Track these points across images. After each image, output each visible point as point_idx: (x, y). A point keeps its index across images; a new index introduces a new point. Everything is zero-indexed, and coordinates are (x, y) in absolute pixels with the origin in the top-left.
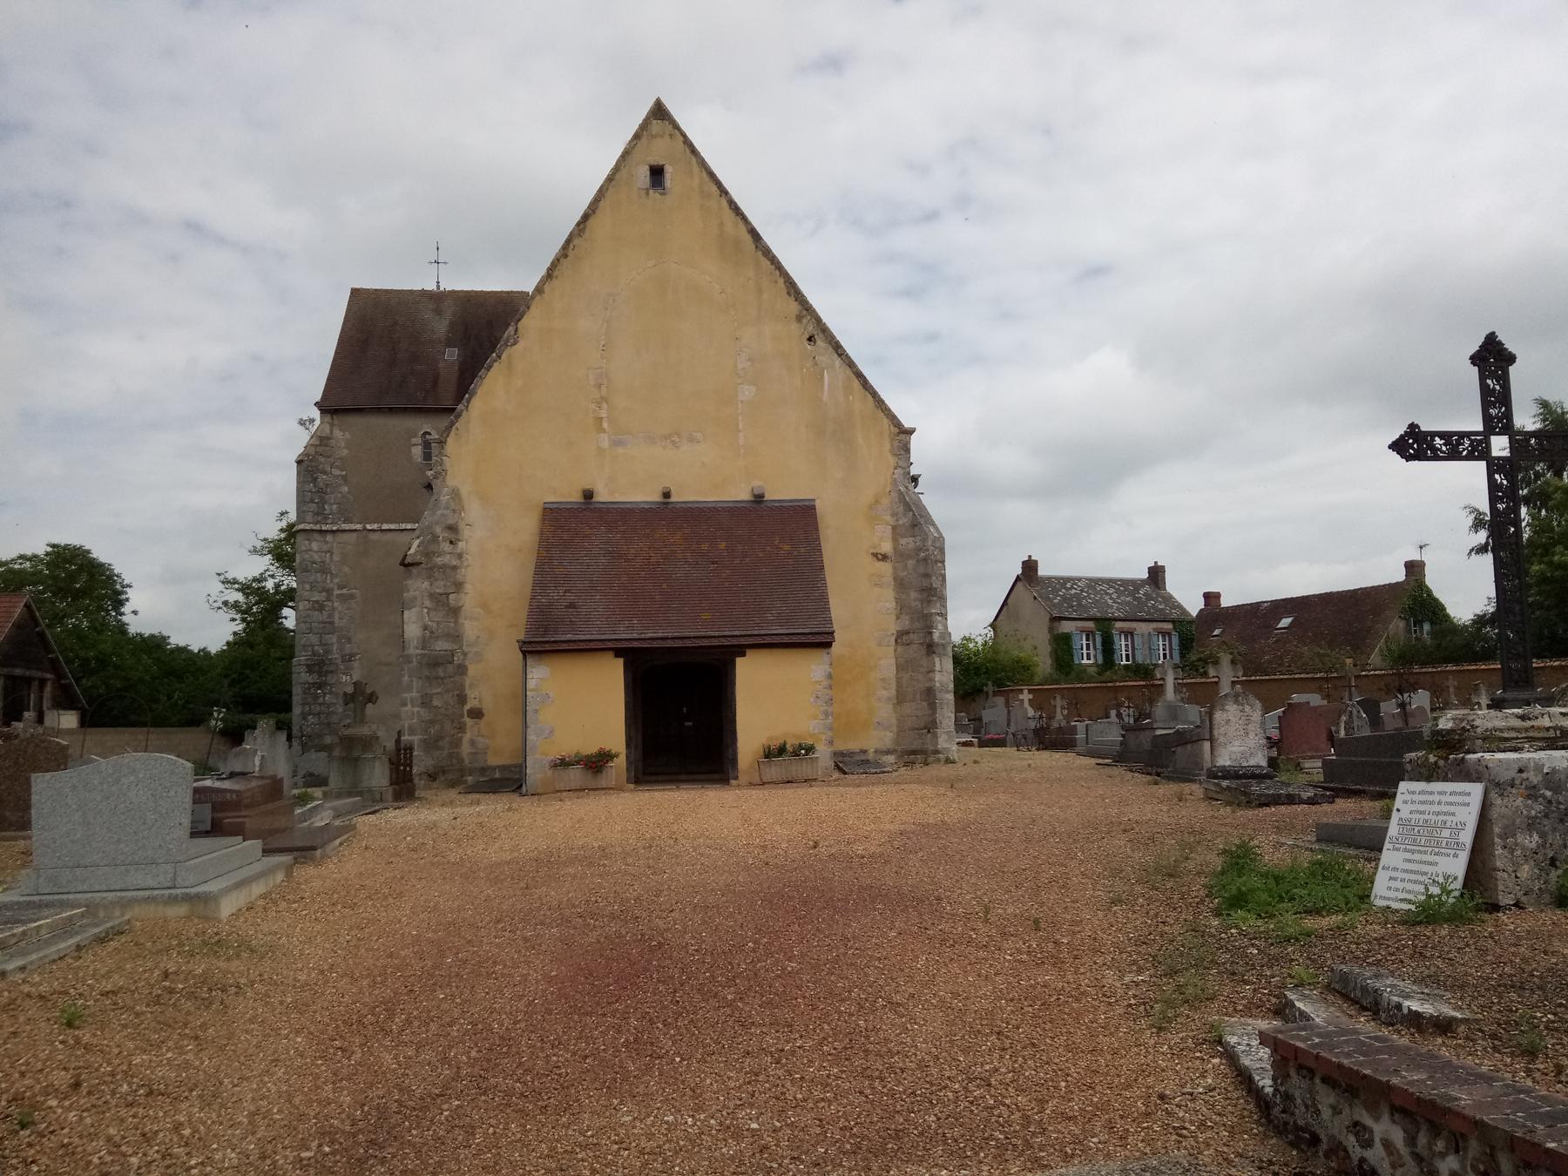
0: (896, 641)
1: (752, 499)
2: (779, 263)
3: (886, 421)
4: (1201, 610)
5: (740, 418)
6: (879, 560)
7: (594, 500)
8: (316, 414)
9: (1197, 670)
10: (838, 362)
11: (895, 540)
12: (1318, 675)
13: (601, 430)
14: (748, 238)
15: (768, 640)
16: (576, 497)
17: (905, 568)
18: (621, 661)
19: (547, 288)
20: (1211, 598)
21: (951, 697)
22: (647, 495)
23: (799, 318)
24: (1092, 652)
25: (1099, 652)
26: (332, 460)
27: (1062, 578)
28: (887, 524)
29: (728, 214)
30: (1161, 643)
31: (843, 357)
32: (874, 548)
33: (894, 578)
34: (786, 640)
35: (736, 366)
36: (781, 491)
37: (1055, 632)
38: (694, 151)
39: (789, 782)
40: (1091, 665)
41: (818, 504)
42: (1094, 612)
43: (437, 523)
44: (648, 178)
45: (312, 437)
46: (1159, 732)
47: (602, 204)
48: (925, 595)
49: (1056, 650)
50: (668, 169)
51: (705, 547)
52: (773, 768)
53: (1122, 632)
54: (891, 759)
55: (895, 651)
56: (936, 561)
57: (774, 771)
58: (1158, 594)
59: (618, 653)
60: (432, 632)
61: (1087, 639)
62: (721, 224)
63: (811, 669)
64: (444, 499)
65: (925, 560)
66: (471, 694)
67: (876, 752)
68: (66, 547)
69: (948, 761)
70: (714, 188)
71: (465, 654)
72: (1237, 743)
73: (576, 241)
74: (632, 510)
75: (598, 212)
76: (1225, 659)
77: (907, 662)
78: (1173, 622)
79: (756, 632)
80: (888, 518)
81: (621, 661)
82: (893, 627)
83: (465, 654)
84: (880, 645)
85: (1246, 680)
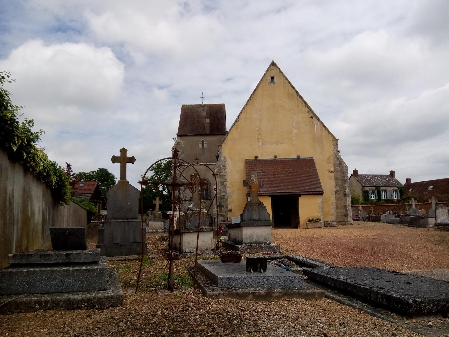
0: (335, 193)
1: (297, 157)
2: (303, 99)
3: (331, 137)
4: (405, 184)
5: (294, 137)
6: (330, 172)
7: (258, 158)
8: (176, 137)
9: (406, 201)
10: (318, 123)
11: (334, 167)
12: (445, 202)
13: (259, 141)
14: (295, 93)
15: (307, 193)
16: (253, 158)
17: (338, 175)
18: (270, 198)
19: (246, 108)
20: (408, 180)
21: (351, 207)
22: (270, 157)
23: (308, 112)
24: (374, 196)
25: (376, 195)
26: (180, 148)
27: (365, 175)
28: (332, 163)
29: (290, 87)
30: (394, 193)
31: (320, 122)
32: (329, 169)
33: (335, 177)
34: (311, 193)
35: (292, 125)
36: (305, 155)
37: (364, 190)
38: (282, 73)
39: (314, 228)
40: (374, 200)
41: (314, 158)
42: (375, 184)
43: (221, 165)
44: (270, 80)
45: (175, 143)
46: (411, 216)
47: (259, 87)
48: (343, 182)
49: (364, 195)
50: (275, 77)
51: (287, 170)
52: (311, 225)
53: (383, 190)
54: (335, 223)
55: (335, 196)
56: (346, 173)
57: (310, 225)
58: (393, 180)
59: (270, 196)
60: (221, 191)
61: (373, 192)
62: (289, 90)
63: (318, 200)
64: (222, 159)
65: (343, 172)
66: (229, 206)
67: (331, 221)
68: (103, 169)
69: (351, 224)
70: (287, 81)
71: (227, 196)
72: (442, 217)
73: (253, 96)
74: (267, 161)
75: (258, 89)
76: (413, 199)
77: (339, 199)
78: (398, 187)
79: (303, 191)
80: (332, 162)
81: (270, 198)
82: (334, 189)
83: (227, 196)
84: (331, 194)
85: (423, 204)
